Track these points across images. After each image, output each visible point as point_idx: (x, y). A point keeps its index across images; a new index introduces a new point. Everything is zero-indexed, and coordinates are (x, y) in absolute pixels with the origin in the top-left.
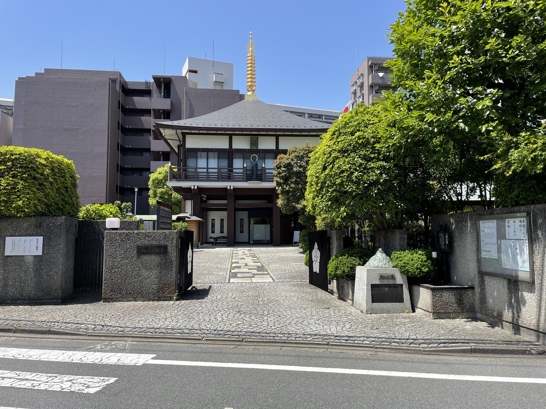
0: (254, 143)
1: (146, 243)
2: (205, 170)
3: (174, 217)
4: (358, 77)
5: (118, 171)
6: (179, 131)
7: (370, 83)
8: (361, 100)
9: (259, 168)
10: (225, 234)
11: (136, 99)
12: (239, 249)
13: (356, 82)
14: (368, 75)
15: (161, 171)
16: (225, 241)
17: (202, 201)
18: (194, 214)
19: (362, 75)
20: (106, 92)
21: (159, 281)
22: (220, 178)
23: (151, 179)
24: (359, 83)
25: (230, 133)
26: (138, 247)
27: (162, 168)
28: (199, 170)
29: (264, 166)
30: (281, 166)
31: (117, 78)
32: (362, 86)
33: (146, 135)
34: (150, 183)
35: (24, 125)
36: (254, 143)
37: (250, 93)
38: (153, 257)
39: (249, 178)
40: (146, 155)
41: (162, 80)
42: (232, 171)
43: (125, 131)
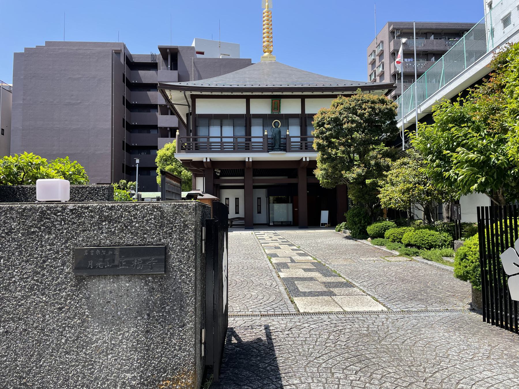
0: (276, 107)
1: (104, 239)
2: (219, 140)
3: (184, 194)
4: (376, 46)
5: (124, 149)
6: (188, 93)
7: (391, 50)
8: (381, 69)
9: (282, 137)
10: (242, 214)
11: (142, 73)
12: (262, 232)
13: (374, 51)
14: (389, 42)
15: (167, 148)
16: (242, 222)
17: (216, 177)
18: (207, 191)
19: (382, 42)
20: (108, 62)
21: (146, 359)
22: (236, 149)
23: (159, 155)
24: (378, 51)
25: (248, 95)
26: (77, 253)
27: (170, 144)
28: (211, 140)
29: (288, 133)
30: (324, 123)
31: (121, 50)
32: (381, 55)
33: (152, 112)
34: (157, 160)
35: (24, 100)
36: (276, 107)
37: (267, 54)
38: (125, 283)
39: (271, 147)
40: (154, 132)
41: (168, 51)
42: (251, 141)
43: (131, 107)
